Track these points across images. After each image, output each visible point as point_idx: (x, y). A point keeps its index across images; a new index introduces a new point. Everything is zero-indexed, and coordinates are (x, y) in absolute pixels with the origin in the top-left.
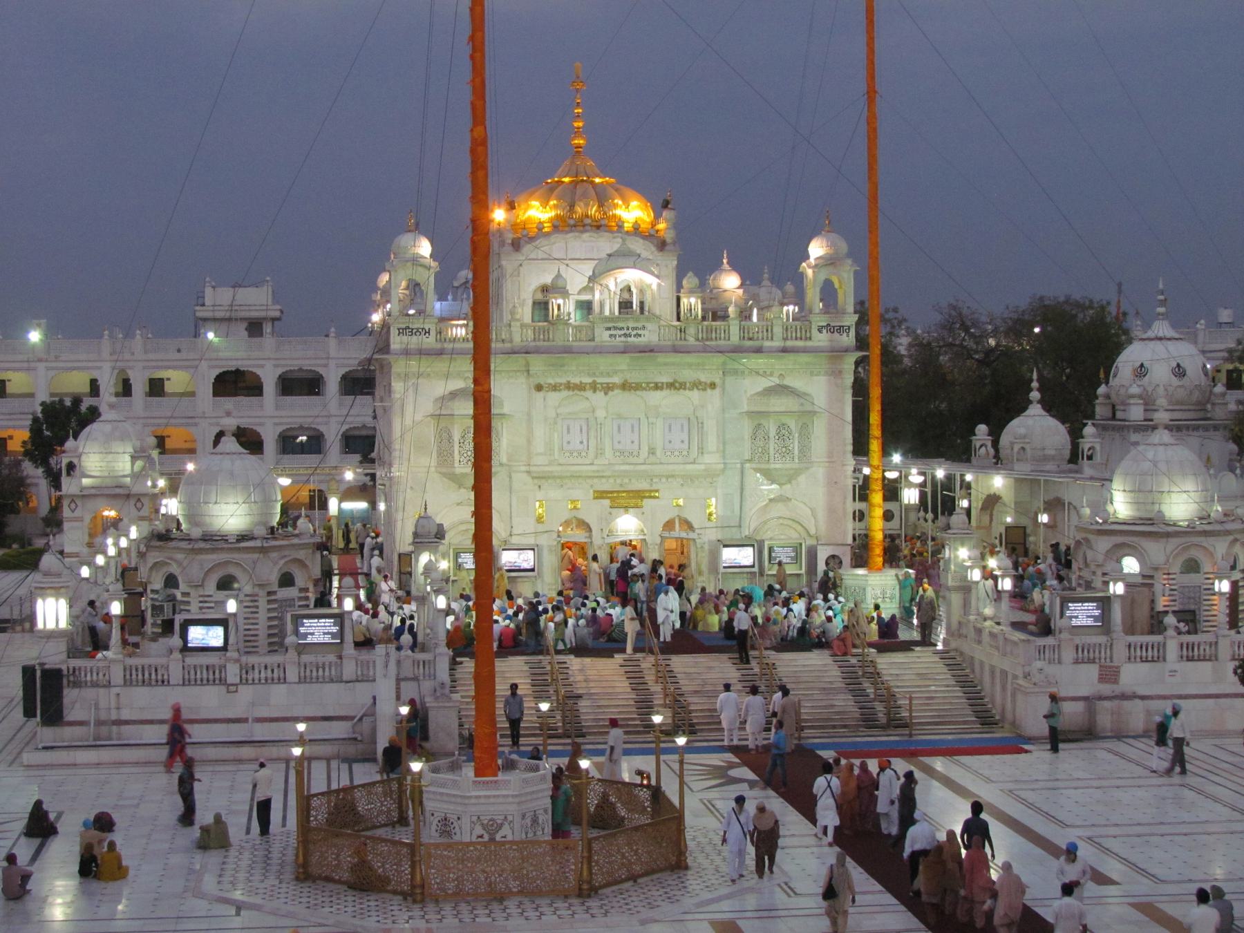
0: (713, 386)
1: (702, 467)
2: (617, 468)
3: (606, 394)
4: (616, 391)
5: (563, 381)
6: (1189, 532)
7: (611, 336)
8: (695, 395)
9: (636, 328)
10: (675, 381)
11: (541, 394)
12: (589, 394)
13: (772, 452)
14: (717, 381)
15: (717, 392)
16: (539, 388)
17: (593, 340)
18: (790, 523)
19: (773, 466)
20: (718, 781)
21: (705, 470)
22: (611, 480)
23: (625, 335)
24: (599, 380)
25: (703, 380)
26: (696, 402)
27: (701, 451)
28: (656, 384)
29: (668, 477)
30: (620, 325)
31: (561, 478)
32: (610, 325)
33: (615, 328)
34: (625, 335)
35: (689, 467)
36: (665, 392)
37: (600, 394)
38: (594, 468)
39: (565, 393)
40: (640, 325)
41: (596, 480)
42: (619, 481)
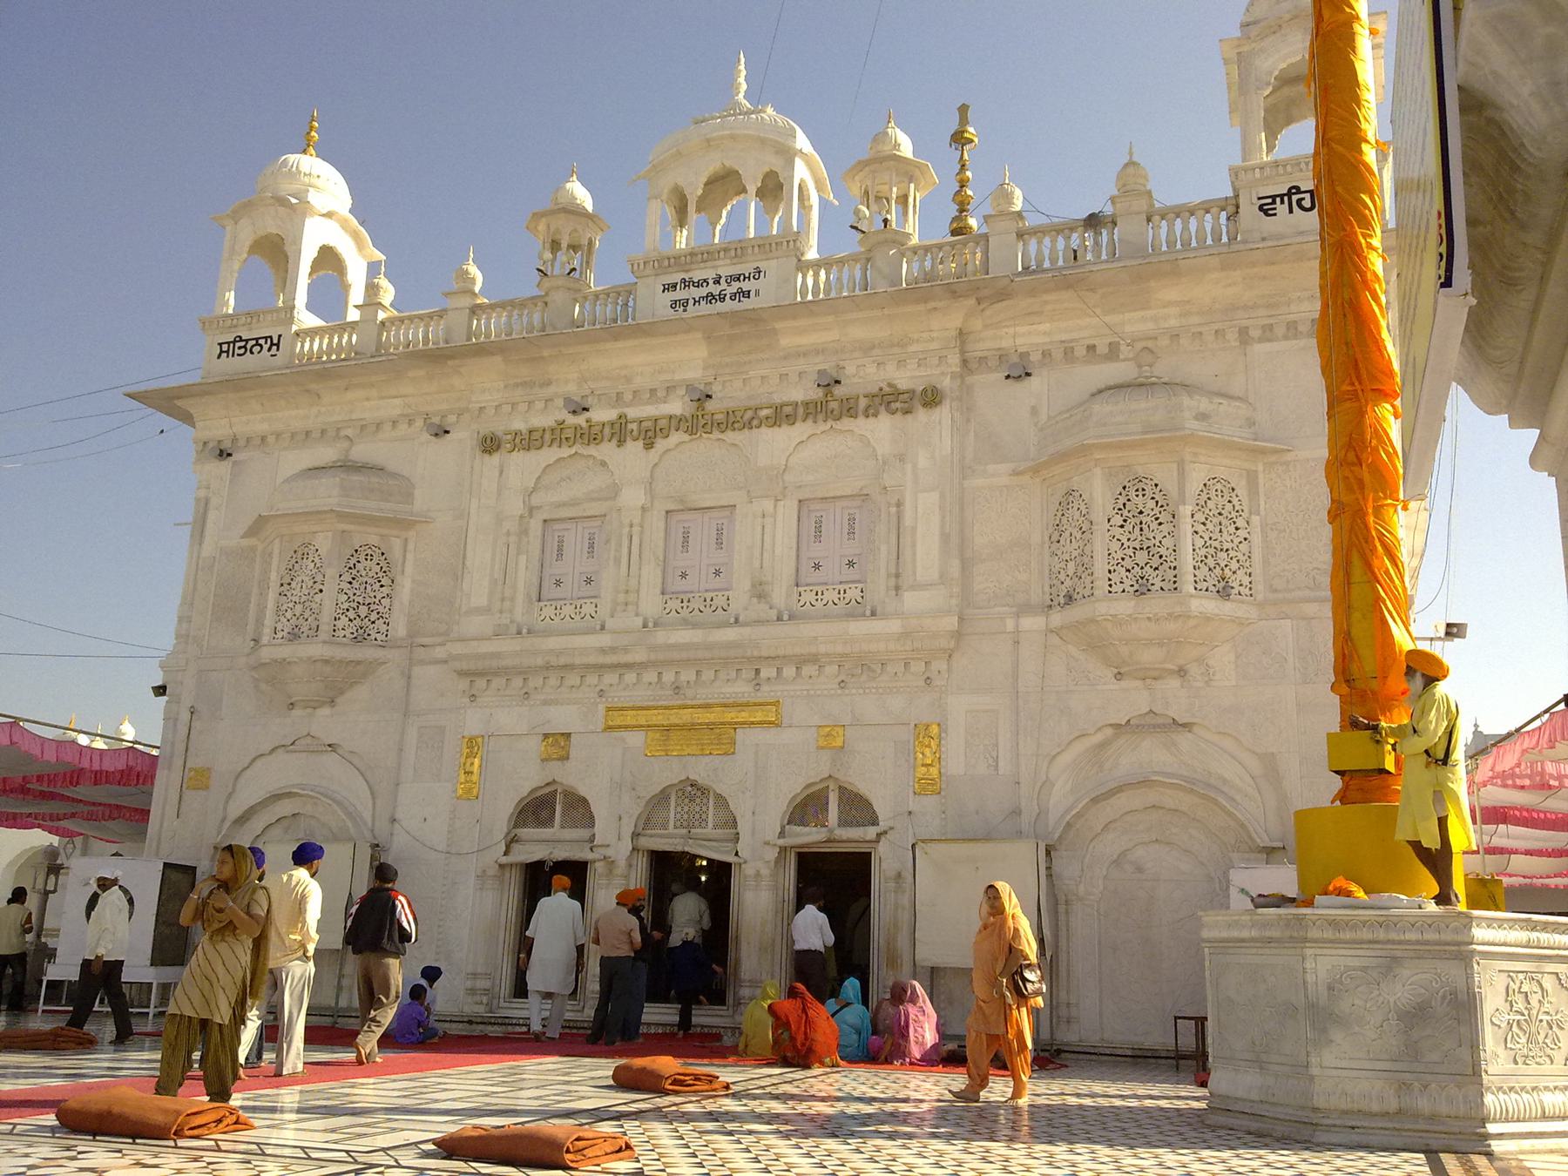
0: (931, 398)
1: (894, 626)
2: (661, 637)
3: (649, 446)
4: (676, 437)
6: (370, 361)
8: (881, 429)
11: (495, 459)
12: (607, 450)
14: (946, 383)
15: (943, 414)
20: (27, 726)
21: (905, 635)
22: (651, 676)
23: (710, 298)
24: (632, 413)
25: (903, 385)
26: (884, 449)
28: (778, 409)
29: (801, 662)
30: (697, 275)
31: (525, 673)
32: (676, 278)
33: (686, 283)
34: (710, 298)
35: (858, 628)
36: (801, 430)
37: (634, 447)
38: (604, 640)
40: (747, 268)
41: (610, 678)
42: (669, 677)
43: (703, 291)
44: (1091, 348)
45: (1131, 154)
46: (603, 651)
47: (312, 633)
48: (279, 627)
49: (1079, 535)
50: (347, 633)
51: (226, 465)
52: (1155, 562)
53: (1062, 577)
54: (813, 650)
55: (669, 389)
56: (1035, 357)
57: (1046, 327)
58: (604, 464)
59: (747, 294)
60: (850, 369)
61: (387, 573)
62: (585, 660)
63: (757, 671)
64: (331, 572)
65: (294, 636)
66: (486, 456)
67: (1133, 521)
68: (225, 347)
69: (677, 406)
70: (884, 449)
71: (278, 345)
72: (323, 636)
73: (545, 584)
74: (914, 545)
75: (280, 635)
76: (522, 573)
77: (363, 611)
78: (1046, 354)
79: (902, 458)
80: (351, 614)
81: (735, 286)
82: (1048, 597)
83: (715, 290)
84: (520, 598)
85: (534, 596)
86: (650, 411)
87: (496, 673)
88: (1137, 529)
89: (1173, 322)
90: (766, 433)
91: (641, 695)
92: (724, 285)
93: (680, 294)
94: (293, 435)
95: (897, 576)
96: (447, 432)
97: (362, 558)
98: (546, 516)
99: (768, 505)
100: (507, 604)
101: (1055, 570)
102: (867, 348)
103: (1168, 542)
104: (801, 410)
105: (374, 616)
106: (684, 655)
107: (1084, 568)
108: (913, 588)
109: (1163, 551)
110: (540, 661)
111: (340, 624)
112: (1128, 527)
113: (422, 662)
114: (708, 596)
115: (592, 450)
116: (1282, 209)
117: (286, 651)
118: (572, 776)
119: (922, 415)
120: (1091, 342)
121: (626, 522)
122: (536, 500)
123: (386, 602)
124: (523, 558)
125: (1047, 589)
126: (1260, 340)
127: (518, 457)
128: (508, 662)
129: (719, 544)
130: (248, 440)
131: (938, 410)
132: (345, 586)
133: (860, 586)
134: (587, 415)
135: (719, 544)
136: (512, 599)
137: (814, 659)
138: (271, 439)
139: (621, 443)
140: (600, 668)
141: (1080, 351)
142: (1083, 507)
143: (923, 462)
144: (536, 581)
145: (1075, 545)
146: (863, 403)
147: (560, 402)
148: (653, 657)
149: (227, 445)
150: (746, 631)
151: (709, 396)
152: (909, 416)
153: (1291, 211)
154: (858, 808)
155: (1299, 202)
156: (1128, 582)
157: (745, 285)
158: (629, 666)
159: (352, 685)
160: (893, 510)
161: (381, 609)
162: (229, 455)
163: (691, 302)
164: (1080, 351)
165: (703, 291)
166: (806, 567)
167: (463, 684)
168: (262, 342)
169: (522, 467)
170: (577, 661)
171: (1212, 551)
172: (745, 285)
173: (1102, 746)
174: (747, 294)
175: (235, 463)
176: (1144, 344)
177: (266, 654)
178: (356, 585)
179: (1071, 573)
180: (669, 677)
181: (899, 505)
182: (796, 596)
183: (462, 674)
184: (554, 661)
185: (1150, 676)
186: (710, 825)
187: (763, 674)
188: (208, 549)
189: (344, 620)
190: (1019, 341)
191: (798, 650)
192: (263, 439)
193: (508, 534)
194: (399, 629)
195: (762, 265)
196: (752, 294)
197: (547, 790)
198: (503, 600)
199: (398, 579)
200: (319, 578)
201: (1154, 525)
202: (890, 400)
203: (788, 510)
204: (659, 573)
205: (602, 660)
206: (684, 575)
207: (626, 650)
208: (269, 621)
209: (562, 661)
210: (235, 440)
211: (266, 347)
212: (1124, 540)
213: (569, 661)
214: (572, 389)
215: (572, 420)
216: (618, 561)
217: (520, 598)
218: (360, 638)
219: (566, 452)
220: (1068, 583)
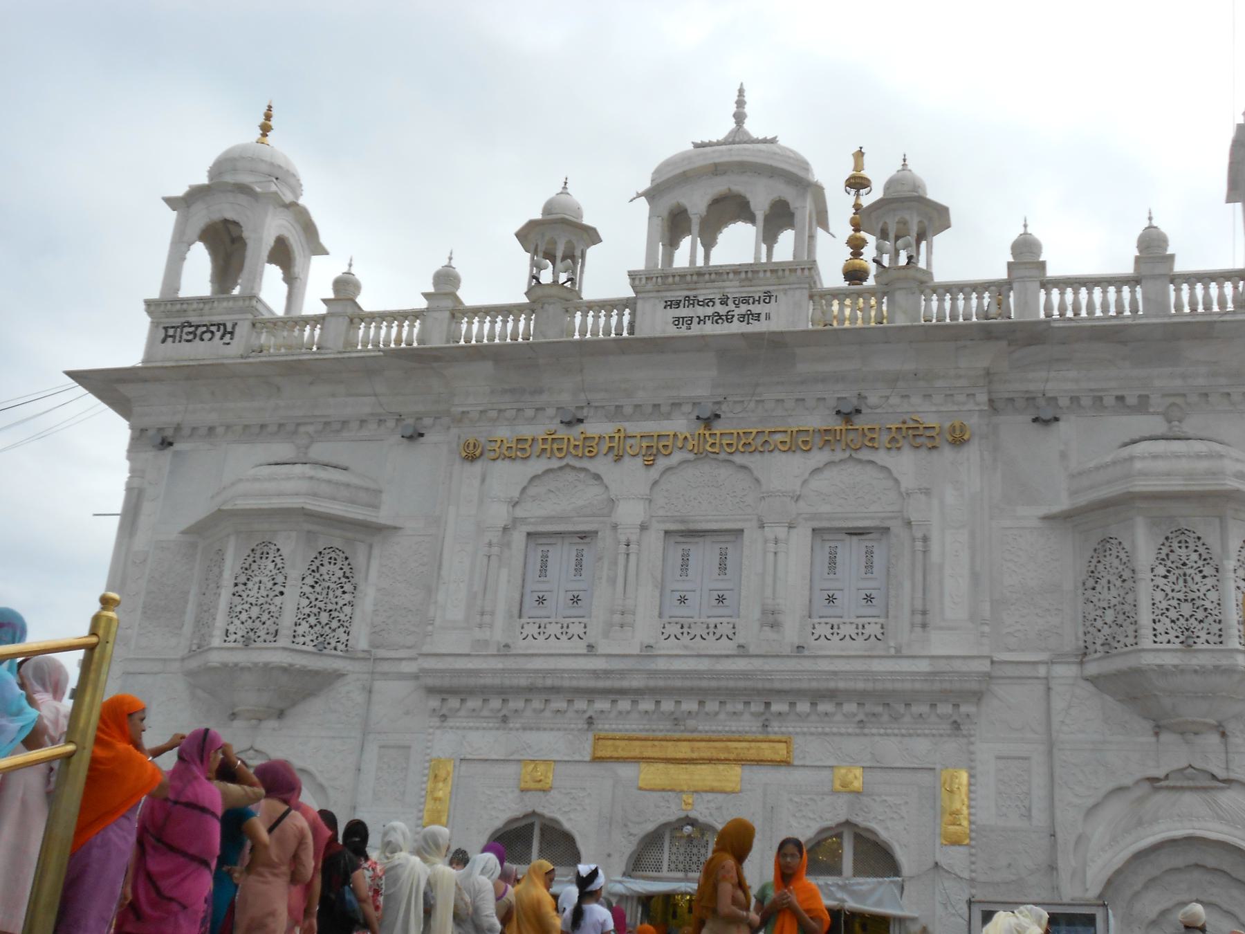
0: (958, 440)
7: (677, 321)
9: (746, 301)
11: (478, 467)
12: (602, 465)
14: (973, 422)
15: (972, 452)
17: (1095, 522)
19: (1148, 660)
22: (647, 705)
24: (633, 428)
25: (930, 420)
27: (923, 619)
29: (817, 696)
31: (504, 693)
32: (680, 294)
33: (691, 301)
37: (633, 466)
41: (602, 705)
43: (709, 311)
44: (1120, 399)
46: (595, 673)
47: (270, 637)
48: (232, 629)
49: (1119, 583)
50: (307, 639)
51: (169, 452)
52: (1200, 614)
53: (1099, 623)
54: (832, 685)
55: (676, 405)
56: (1064, 402)
57: (1073, 374)
58: (597, 477)
60: (873, 399)
62: (575, 683)
63: (768, 704)
64: (294, 574)
65: (247, 642)
66: (467, 466)
67: (1177, 572)
68: (171, 332)
69: (680, 425)
71: (232, 333)
72: (283, 641)
73: (527, 599)
75: (232, 637)
77: (324, 617)
78: (1075, 400)
80: (312, 620)
81: (743, 308)
82: (1082, 644)
83: (722, 310)
85: (516, 612)
86: (651, 427)
88: (325, 592)
89: (1201, 381)
91: (633, 725)
92: (731, 306)
93: (683, 312)
94: (246, 427)
95: (924, 613)
96: (421, 435)
97: (326, 561)
98: (531, 529)
99: (781, 532)
100: (487, 618)
101: (1091, 617)
102: (893, 380)
105: (335, 624)
106: (688, 683)
107: (1128, 616)
109: (1207, 604)
110: (523, 682)
111: (300, 630)
112: (1172, 578)
113: (385, 675)
114: (712, 621)
117: (242, 657)
118: (555, 808)
119: (948, 453)
120: (1119, 393)
121: (623, 538)
123: (347, 610)
124: (504, 573)
125: (1081, 634)
127: (502, 466)
128: (488, 681)
129: (723, 567)
130: (194, 429)
132: (307, 589)
133: (881, 620)
134: (581, 428)
135: (723, 567)
136: (492, 613)
138: (220, 430)
139: (619, 458)
140: (591, 694)
141: (1109, 401)
142: (1123, 555)
144: (517, 596)
145: (1114, 592)
147: (551, 411)
148: (652, 683)
149: (169, 433)
150: (757, 664)
151: (718, 416)
152: (935, 453)
156: (1173, 633)
157: (756, 308)
158: (622, 692)
159: (304, 698)
160: (919, 545)
161: (342, 617)
162: (171, 444)
163: (696, 320)
164: (1109, 401)
165: (709, 311)
166: (530, 600)
167: (434, 703)
168: (214, 329)
170: (566, 683)
171: (1175, 603)
172: (756, 308)
175: (176, 454)
176: (1172, 400)
177: (215, 658)
178: (318, 589)
179: (1109, 619)
181: (925, 539)
182: (518, 629)
183: (431, 691)
184: (539, 683)
185: (1187, 731)
186: (665, 867)
188: (141, 541)
189: (304, 627)
190: (1050, 386)
191: (814, 685)
192: (211, 429)
193: (490, 544)
194: (361, 639)
196: (763, 317)
197: (523, 823)
198: (482, 614)
199: (361, 587)
200: (280, 579)
201: (1198, 578)
202: (916, 436)
203: (800, 540)
204: (657, 594)
205: (592, 684)
206: (683, 600)
208: (221, 621)
209: (549, 682)
210: (178, 428)
211: (218, 335)
212: (1168, 590)
213: (558, 683)
214: (566, 399)
215: (563, 433)
216: (612, 581)
218: (322, 646)
220: (1106, 630)
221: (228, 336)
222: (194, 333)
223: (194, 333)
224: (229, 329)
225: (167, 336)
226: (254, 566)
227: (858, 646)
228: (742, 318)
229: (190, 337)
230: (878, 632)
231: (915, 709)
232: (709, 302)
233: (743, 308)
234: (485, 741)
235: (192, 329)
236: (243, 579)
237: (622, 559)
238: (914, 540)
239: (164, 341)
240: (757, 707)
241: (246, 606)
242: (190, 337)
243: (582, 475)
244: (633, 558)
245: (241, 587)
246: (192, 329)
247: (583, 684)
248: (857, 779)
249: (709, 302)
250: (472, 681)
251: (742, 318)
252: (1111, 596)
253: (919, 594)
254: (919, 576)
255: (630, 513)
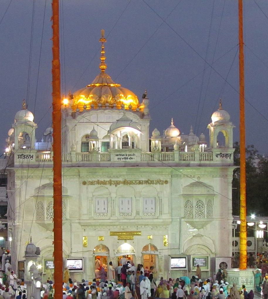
0: (166, 182)
1: (162, 220)
2: (121, 221)
3: (116, 186)
4: (121, 185)
5: (96, 180)
7: (118, 158)
10: (149, 180)
11: (85, 186)
12: (108, 186)
13: (194, 213)
14: (168, 180)
15: (168, 185)
16: (84, 183)
18: (203, 247)
19: (195, 220)
21: (163, 222)
22: (119, 227)
23: (125, 158)
24: (113, 180)
25: (162, 179)
27: (161, 213)
28: (140, 181)
30: (123, 153)
32: (118, 153)
33: (120, 155)
34: (125, 158)
35: (155, 220)
36: (144, 185)
37: (113, 186)
39: (97, 186)
40: (132, 153)
41: (111, 227)
43: (124, 157)
45: (94, 128)
46: (110, 222)
52: (202, 213)
59: (132, 158)
61: (70, 283)
62: (107, 224)
63: (138, 226)
66: (84, 185)
70: (159, 190)
71: (32, 157)
74: (164, 207)
76: (92, 208)
79: (162, 192)
81: (129, 157)
83: (126, 157)
84: (92, 212)
87: (89, 225)
90: (138, 185)
92: (127, 156)
95: (161, 212)
103: (203, 210)
104: (144, 182)
108: (164, 214)
110: (98, 224)
113: (73, 223)
115: (105, 186)
116: (219, 156)
122: (94, 194)
124: (92, 205)
126: (215, 177)
128: (92, 224)
131: (167, 184)
137: (147, 225)
139: (111, 185)
143: (165, 193)
146: (155, 182)
153: (220, 157)
154: (155, 248)
155: (222, 155)
165: (124, 157)
168: (28, 156)
169: (91, 188)
172: (132, 157)
173: (192, 238)
174: (132, 158)
179: (189, 213)
180: (122, 227)
187: (139, 227)
195: (135, 153)
205: (110, 224)
207: (115, 223)
209: (103, 224)
217: (92, 212)
219: (99, 185)
221: (32, 158)
222: (24, 157)
223: (24, 157)
224: (32, 156)
225: (19, 157)
226: (50, 206)
227: (151, 217)
228: (130, 159)
229: (24, 158)
230: (154, 214)
231: (160, 227)
232: (123, 155)
233: (129, 157)
234: (92, 233)
235: (24, 156)
236: (48, 208)
237: (113, 203)
238: (159, 200)
239: (18, 158)
240: (136, 227)
241: (50, 213)
242: (24, 158)
243: (104, 188)
244: (114, 203)
245: (48, 210)
246: (24, 156)
247: (108, 224)
248: (151, 237)
249: (123, 155)
250: (89, 224)
251: (130, 159)
252: (189, 209)
253: (160, 209)
254: (160, 205)
255: (113, 195)
